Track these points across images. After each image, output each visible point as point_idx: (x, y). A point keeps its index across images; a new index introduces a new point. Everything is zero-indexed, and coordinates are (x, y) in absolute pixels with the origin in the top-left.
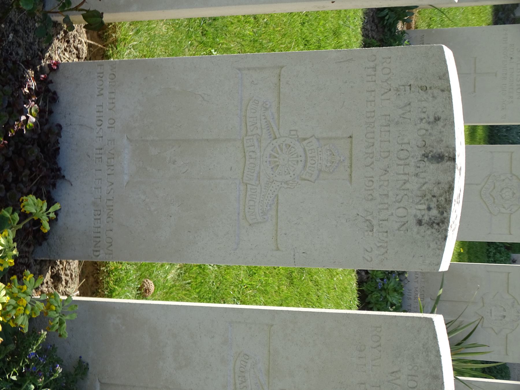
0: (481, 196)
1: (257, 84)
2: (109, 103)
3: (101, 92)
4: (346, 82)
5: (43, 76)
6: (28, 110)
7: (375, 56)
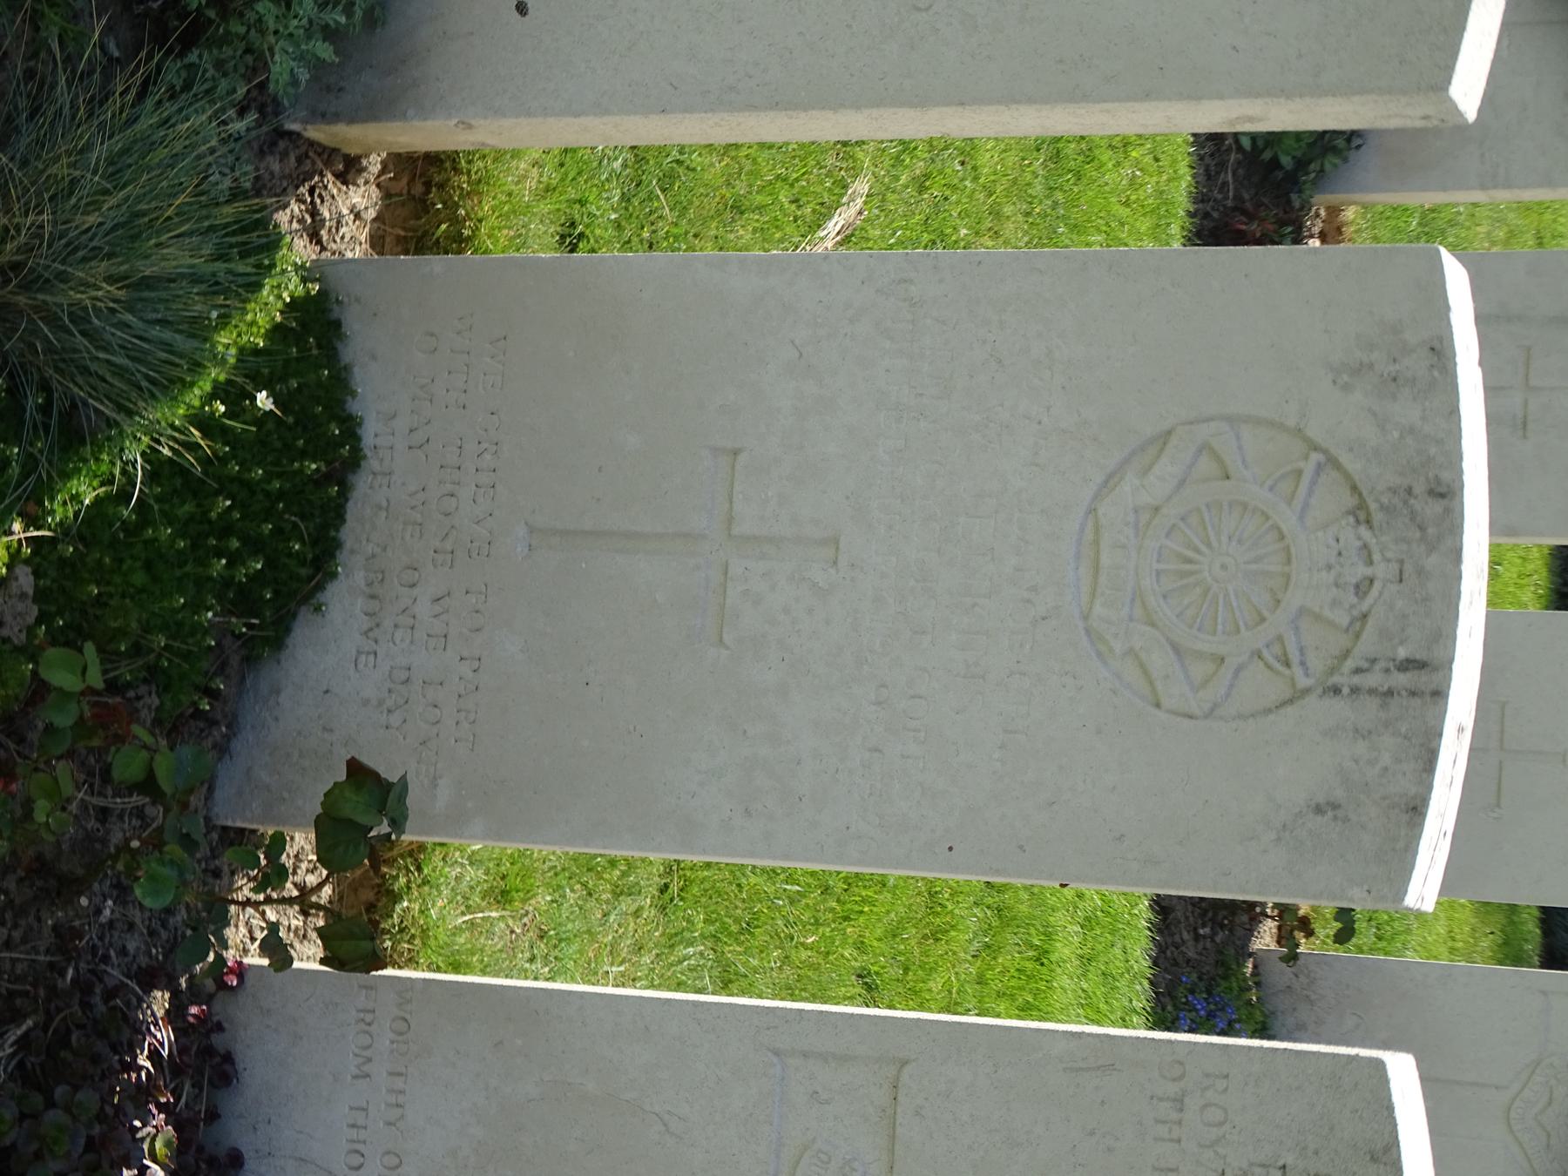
0: (1509, 1125)
1: (827, 1102)
2: (388, 1105)
3: (365, 1068)
4: (1092, 1133)
5: (194, 1010)
6: (146, 1147)
7: (1181, 1063)
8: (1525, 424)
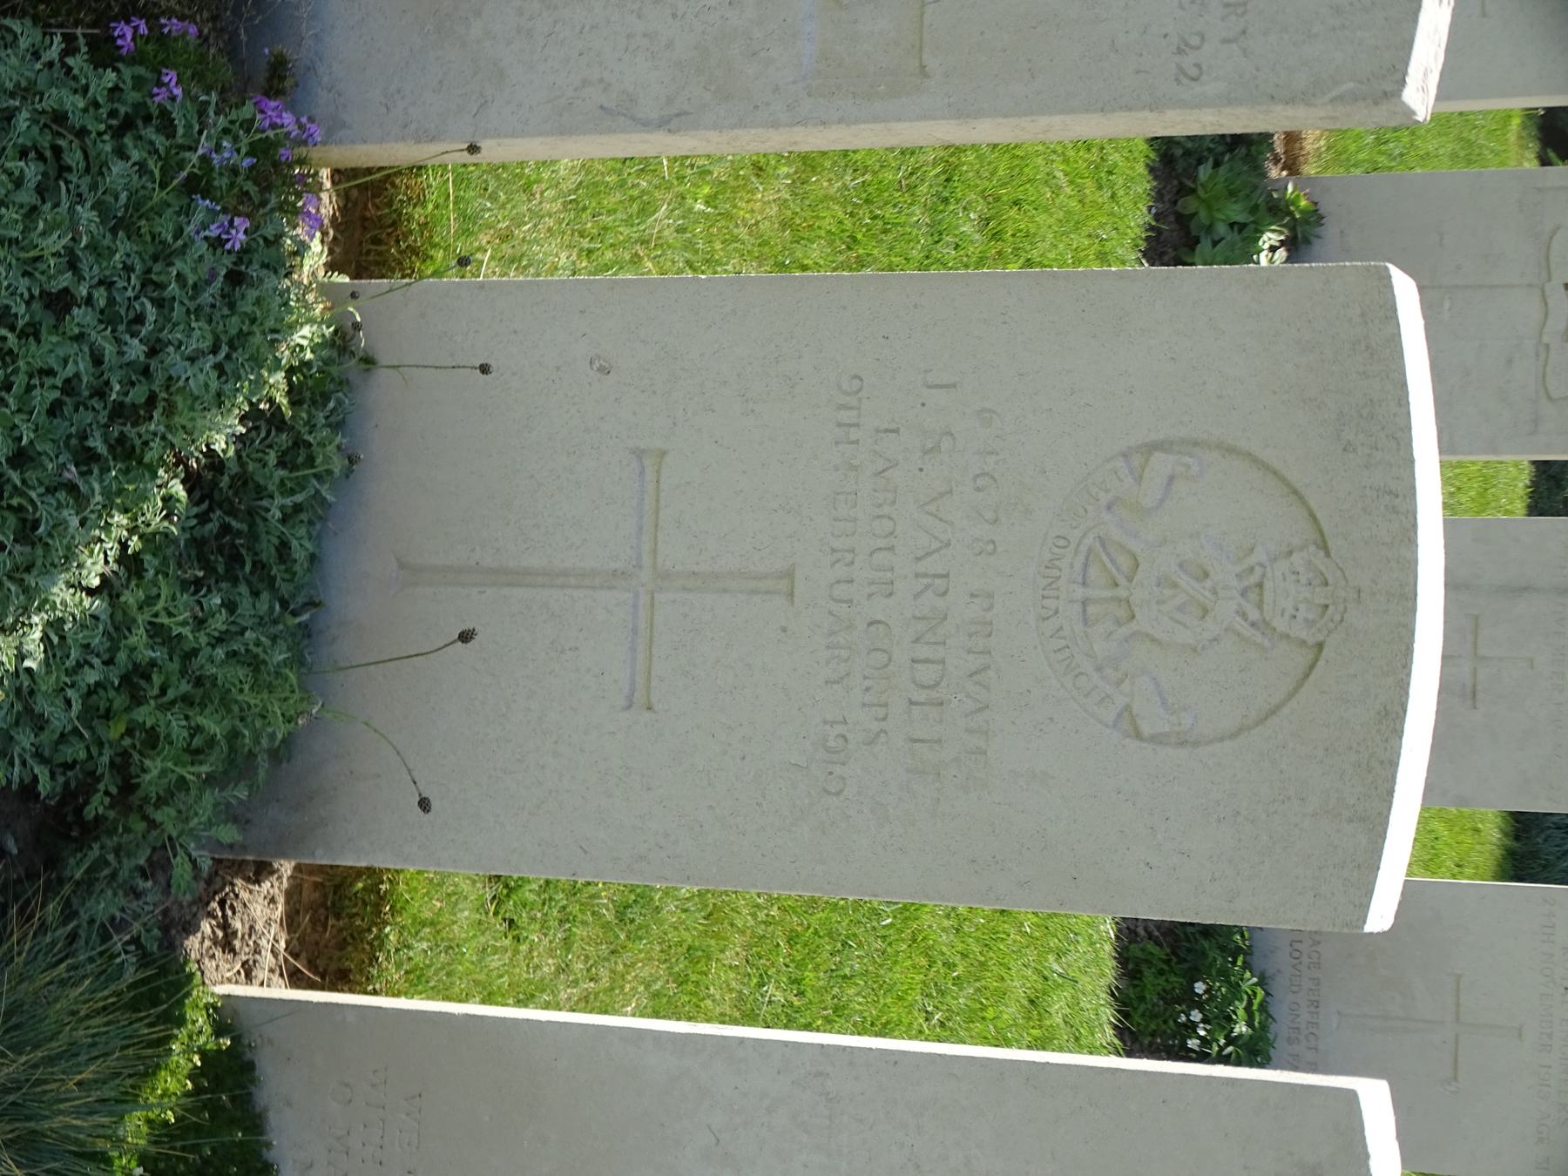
8: (1474, 693)
